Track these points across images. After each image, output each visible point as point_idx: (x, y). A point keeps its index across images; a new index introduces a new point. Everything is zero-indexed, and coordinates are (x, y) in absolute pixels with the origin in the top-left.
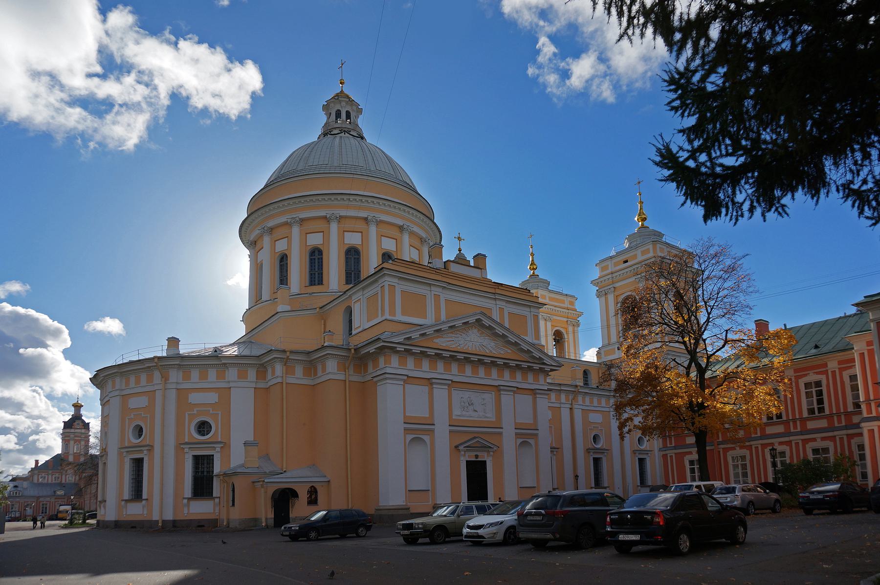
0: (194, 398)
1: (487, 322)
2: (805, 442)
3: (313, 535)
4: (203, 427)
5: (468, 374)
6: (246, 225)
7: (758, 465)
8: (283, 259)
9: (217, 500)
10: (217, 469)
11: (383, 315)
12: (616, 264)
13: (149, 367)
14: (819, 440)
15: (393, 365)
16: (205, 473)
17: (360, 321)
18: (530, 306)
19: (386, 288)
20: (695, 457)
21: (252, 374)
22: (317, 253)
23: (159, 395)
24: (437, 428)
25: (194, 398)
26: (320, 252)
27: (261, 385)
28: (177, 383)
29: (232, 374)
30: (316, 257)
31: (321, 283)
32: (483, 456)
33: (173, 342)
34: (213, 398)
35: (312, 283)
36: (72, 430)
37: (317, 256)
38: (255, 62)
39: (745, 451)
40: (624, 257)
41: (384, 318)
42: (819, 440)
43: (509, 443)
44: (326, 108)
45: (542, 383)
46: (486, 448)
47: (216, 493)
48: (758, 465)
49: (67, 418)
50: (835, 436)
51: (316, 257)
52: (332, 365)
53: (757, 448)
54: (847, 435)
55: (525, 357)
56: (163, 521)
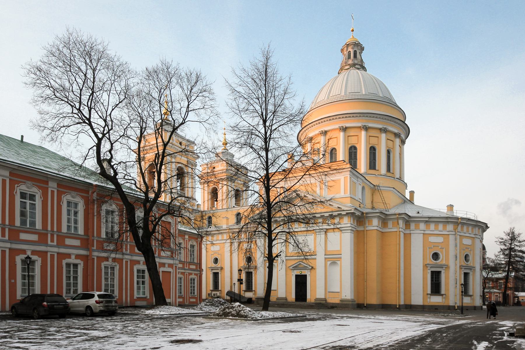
0: (432, 239)
3: (13, 281)
4: (436, 256)
6: (407, 129)
14: (73, 257)
22: (353, 148)
23: (452, 238)
25: (432, 239)
26: (355, 148)
32: (304, 272)
34: (440, 240)
35: (370, 168)
42: (73, 257)
44: (342, 50)
46: (305, 268)
47: (443, 291)
50: (46, 252)
54: (10, 249)
56: (399, 305)
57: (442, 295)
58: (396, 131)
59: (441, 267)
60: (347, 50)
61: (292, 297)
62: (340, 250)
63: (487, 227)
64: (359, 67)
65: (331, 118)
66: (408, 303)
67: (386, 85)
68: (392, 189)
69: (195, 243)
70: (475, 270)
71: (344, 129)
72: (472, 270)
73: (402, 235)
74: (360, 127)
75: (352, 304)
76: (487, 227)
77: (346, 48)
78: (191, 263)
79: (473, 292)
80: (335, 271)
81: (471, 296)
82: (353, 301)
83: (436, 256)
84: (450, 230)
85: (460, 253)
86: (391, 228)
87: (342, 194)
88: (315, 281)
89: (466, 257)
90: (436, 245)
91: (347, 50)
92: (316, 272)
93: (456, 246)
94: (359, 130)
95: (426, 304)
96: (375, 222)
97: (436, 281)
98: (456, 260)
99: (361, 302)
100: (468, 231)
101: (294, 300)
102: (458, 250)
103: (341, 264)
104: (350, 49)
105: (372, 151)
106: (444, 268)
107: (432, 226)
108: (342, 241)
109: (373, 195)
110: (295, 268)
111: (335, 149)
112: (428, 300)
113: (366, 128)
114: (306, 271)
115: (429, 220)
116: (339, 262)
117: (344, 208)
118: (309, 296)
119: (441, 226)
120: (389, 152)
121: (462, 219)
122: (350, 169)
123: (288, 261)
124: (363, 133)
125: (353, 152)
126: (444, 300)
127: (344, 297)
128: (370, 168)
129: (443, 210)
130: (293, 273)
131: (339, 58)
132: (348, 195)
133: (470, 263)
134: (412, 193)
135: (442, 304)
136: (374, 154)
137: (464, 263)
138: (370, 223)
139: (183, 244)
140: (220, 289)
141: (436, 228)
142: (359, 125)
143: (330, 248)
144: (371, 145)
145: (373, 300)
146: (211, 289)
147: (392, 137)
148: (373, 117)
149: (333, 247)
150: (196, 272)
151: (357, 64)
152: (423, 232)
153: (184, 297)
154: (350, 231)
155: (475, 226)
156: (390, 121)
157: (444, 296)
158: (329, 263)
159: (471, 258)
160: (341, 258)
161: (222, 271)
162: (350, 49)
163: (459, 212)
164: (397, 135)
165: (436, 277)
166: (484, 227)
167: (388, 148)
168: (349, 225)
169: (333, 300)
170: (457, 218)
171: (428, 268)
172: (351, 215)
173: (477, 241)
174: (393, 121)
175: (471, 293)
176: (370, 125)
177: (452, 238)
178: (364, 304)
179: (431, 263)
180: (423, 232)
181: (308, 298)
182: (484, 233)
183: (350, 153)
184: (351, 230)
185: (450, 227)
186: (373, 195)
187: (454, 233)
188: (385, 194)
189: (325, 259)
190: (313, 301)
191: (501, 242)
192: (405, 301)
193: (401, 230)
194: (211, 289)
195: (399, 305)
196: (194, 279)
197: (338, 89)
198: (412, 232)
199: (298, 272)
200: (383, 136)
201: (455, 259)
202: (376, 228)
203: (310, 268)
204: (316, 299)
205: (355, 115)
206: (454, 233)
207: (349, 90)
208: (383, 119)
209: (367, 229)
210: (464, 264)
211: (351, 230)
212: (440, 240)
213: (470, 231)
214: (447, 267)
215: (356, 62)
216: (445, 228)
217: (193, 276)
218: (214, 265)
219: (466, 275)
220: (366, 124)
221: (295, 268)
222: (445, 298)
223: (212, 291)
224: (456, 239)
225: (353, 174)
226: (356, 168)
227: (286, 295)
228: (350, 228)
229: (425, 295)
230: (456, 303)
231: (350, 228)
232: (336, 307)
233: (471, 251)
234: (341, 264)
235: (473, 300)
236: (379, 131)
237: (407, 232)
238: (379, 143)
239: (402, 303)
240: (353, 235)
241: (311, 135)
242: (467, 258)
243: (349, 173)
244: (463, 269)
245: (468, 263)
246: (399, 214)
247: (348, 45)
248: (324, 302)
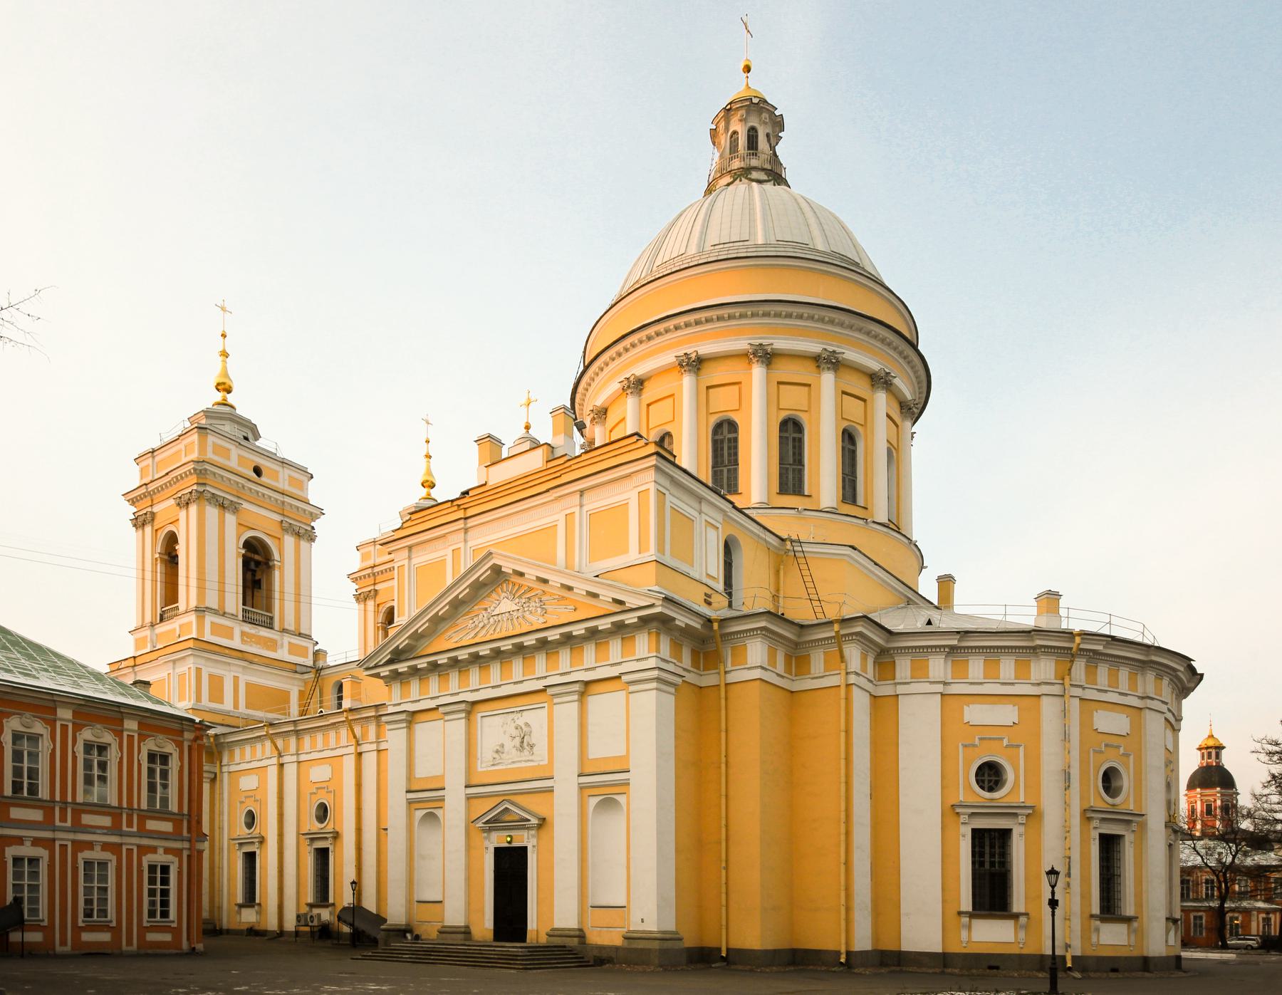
0: (976, 714)
2: (143, 850)
4: (990, 775)
5: (519, 676)
7: (130, 891)
13: (1095, 652)
14: (161, 851)
16: (987, 866)
22: (725, 427)
23: (1049, 708)
25: (976, 714)
26: (732, 426)
28: (945, 684)
32: (523, 839)
34: (1006, 714)
35: (783, 490)
39: (170, 858)
42: (161, 851)
43: (564, 806)
44: (714, 134)
46: (522, 824)
47: (1018, 905)
48: (130, 891)
50: (54, 840)
52: (756, 651)
53: (64, 847)
54: (73, 842)
56: (848, 953)
57: (1016, 917)
58: (874, 365)
59: (1010, 812)
60: (727, 129)
61: (484, 924)
62: (625, 758)
63: (1197, 677)
64: (763, 176)
65: (651, 331)
66: (889, 946)
67: (850, 227)
68: (849, 551)
69: (170, 748)
70: (1143, 827)
71: (696, 364)
72: (1134, 826)
73: (861, 702)
74: (743, 355)
75: (663, 952)
76: (1197, 677)
77: (722, 124)
78: (153, 814)
79: (1139, 905)
80: (610, 831)
81: (1128, 920)
82: (665, 938)
83: (990, 775)
84: (1042, 678)
85: (1084, 762)
86: (821, 673)
87: (633, 556)
88: (551, 869)
89: (1110, 780)
90: (989, 733)
91: (727, 129)
92: (552, 838)
93: (1066, 737)
94: (744, 362)
95: (954, 948)
96: (756, 651)
97: (992, 864)
98: (1067, 788)
99: (710, 942)
100: (1114, 682)
101: (490, 936)
102: (1075, 754)
103: (628, 804)
104: (736, 125)
105: (791, 434)
106: (1021, 819)
107: (976, 667)
108: (633, 723)
109: (777, 572)
110: (494, 824)
111: (669, 434)
112: (964, 934)
113: (768, 357)
114: (525, 833)
115: (967, 643)
116: (622, 799)
117: (632, 602)
118: (532, 924)
119: (1007, 667)
120: (849, 438)
121: (1085, 635)
122: (653, 461)
123: (475, 802)
124: (758, 371)
125: (725, 439)
126: (1022, 935)
127: (636, 926)
128: (783, 490)
129: (1027, 618)
130: (487, 843)
131: (708, 158)
132: (651, 554)
133: (1125, 801)
134: (946, 582)
135: (1017, 951)
136: (798, 444)
137: (1099, 799)
138: (740, 655)
139: (176, 756)
140: (331, 901)
141: (991, 673)
142: (742, 344)
143: (597, 750)
144: (783, 415)
145: (751, 934)
146: (310, 900)
147: (859, 386)
148: (789, 316)
149: (603, 747)
150: (178, 845)
151: (755, 168)
152: (940, 688)
153: (179, 929)
154: (654, 685)
155: (1143, 665)
156: (851, 327)
157: (1023, 920)
158: (593, 801)
159: (1126, 782)
160: (626, 784)
161: (338, 841)
162: (736, 125)
163: (1079, 616)
164: (880, 380)
165: (991, 852)
166: (1182, 675)
167: (845, 424)
168: (652, 663)
169: (605, 936)
170: (1070, 635)
171: (963, 818)
172: (657, 623)
173: (1154, 724)
174: (860, 330)
175: (1129, 910)
176: (780, 344)
177: (1049, 708)
178: (719, 949)
179: (972, 800)
180: (940, 688)
181: (529, 927)
182: (1186, 703)
183: (715, 442)
184: (658, 679)
185: (1044, 668)
186: (777, 572)
187: (1056, 690)
188: (819, 571)
189: (582, 788)
190: (543, 940)
191: (1270, 753)
192: (876, 936)
193: (852, 679)
194: (240, 900)
195: (848, 953)
196: (165, 869)
197: (680, 238)
198: (900, 689)
199: (499, 839)
200: (828, 380)
201: (1062, 785)
202: (757, 674)
203: (534, 821)
204: (554, 933)
205: (724, 312)
206: (1056, 690)
207: (713, 238)
208: (822, 320)
209: (732, 678)
210: (1100, 805)
211: (658, 679)
212: (1006, 714)
213: (1124, 685)
214: (1033, 814)
215: (754, 162)
216: (1022, 673)
217: (160, 858)
218: (317, 826)
219: (1109, 845)
220: (765, 342)
221: (494, 824)
222: (1026, 927)
223: (311, 906)
224: (1065, 712)
225: (673, 481)
226: (733, 488)
227: (581, 921)
228: (655, 673)
229: (951, 918)
230: (1067, 946)
231: (655, 673)
232: (609, 960)
233: (1126, 755)
234: (628, 804)
235: (1140, 934)
236: (811, 366)
237: (885, 690)
238: (813, 404)
239: (863, 941)
240: (670, 700)
241: (599, 402)
242: (1114, 784)
243: (651, 475)
244: (1095, 823)
245: (1118, 800)
246: (844, 622)
247: (728, 111)
248: (574, 942)
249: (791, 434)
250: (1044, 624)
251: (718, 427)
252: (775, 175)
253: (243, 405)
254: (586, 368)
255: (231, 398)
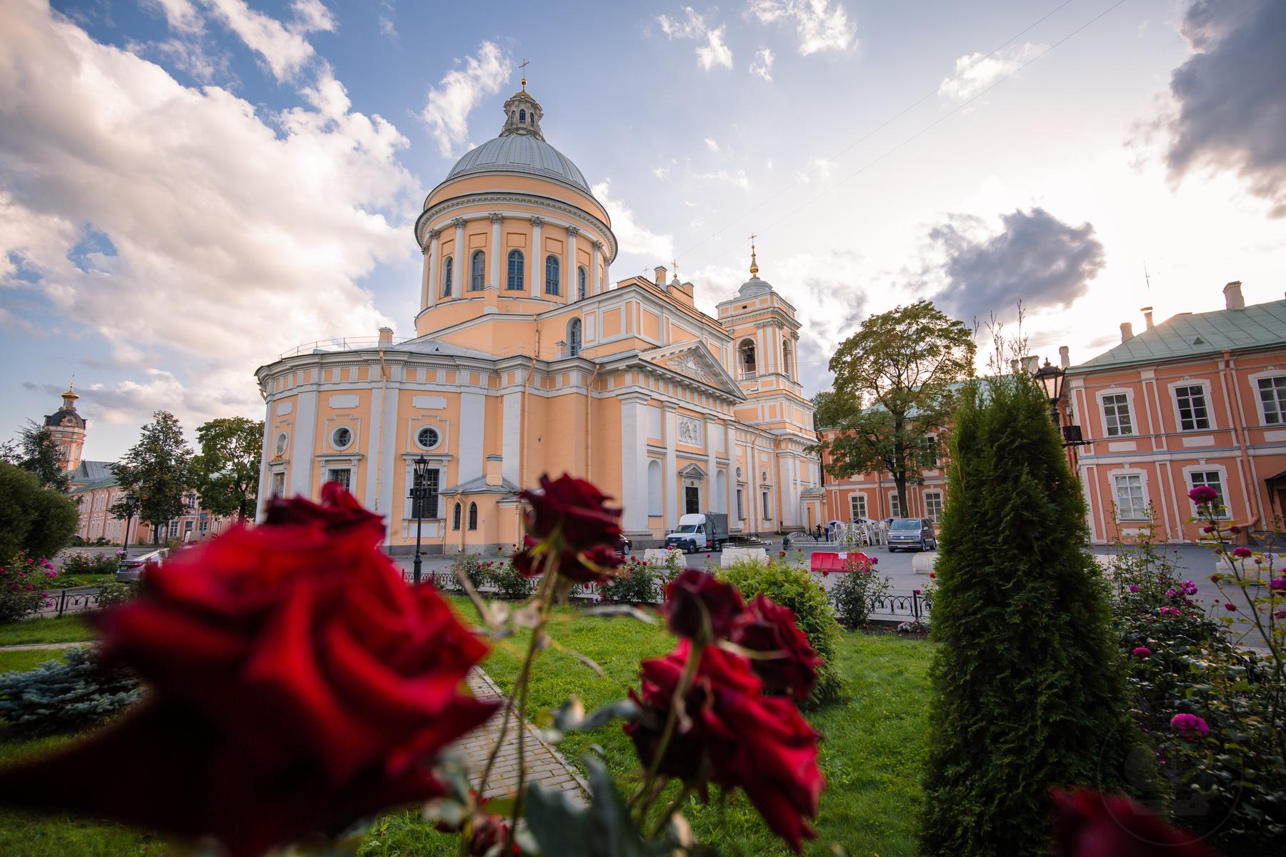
1: (702, 351)
8: (478, 256)
9: (443, 524)
10: (442, 486)
11: (628, 329)
12: (735, 308)
15: (640, 383)
17: (589, 334)
18: (662, 307)
19: (634, 306)
20: (895, 492)
21: (484, 379)
23: (377, 395)
24: (668, 451)
25: (420, 402)
26: (520, 255)
27: (493, 393)
29: (463, 377)
30: (516, 262)
31: (520, 287)
32: (697, 484)
33: (1233, 289)
34: (440, 403)
35: (511, 287)
36: (60, 428)
37: (516, 259)
38: (487, 40)
40: (743, 304)
41: (630, 335)
45: (727, 413)
47: (440, 514)
49: (52, 412)
51: (516, 262)
55: (721, 387)
105: (552, 263)
106: (445, 463)
107: (421, 374)
110: (689, 476)
128: (548, 291)
133: (353, 447)
199: (688, 483)
200: (537, 231)
202: (574, 390)
212: (440, 403)
236: (527, 225)
249: (552, 263)
250: (385, 346)
251: (512, 254)
252: (535, 134)
253: (762, 275)
254: (425, 213)
255: (758, 275)
